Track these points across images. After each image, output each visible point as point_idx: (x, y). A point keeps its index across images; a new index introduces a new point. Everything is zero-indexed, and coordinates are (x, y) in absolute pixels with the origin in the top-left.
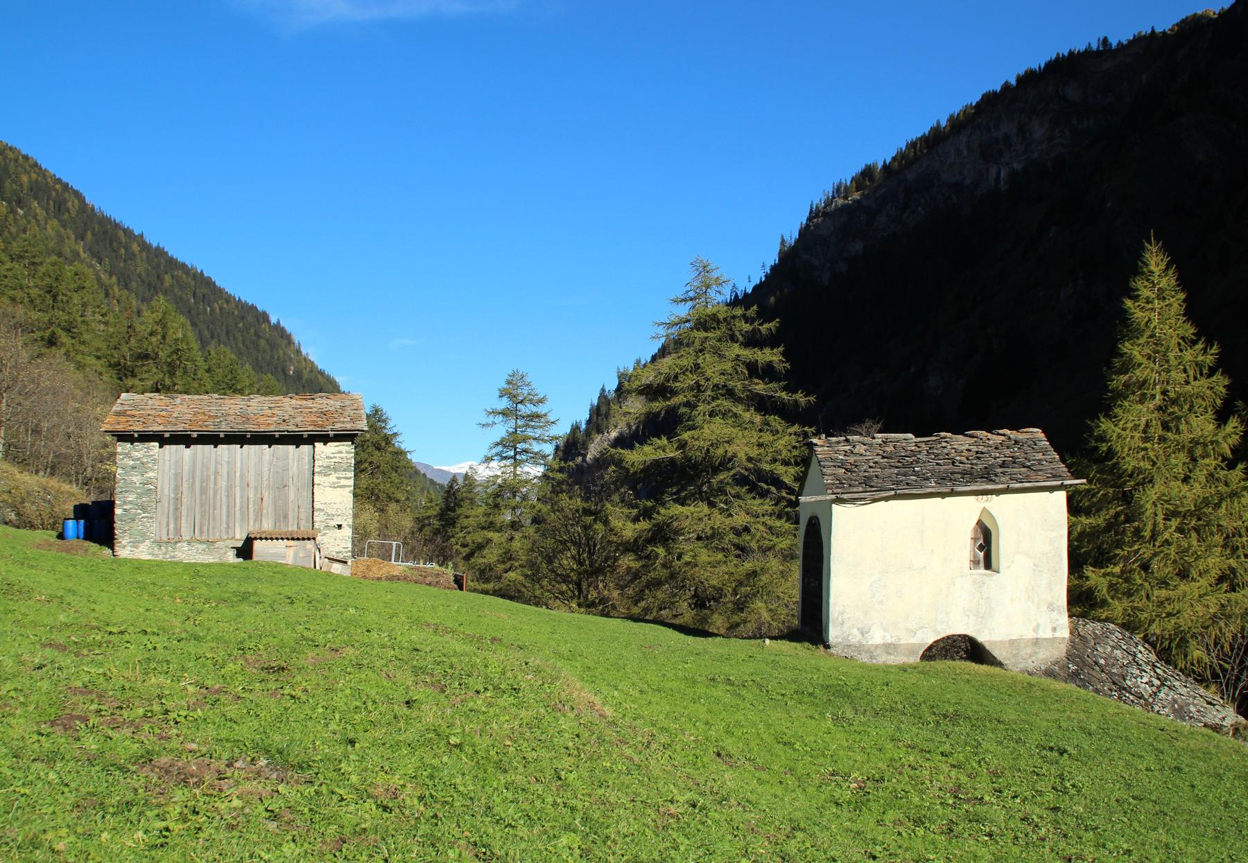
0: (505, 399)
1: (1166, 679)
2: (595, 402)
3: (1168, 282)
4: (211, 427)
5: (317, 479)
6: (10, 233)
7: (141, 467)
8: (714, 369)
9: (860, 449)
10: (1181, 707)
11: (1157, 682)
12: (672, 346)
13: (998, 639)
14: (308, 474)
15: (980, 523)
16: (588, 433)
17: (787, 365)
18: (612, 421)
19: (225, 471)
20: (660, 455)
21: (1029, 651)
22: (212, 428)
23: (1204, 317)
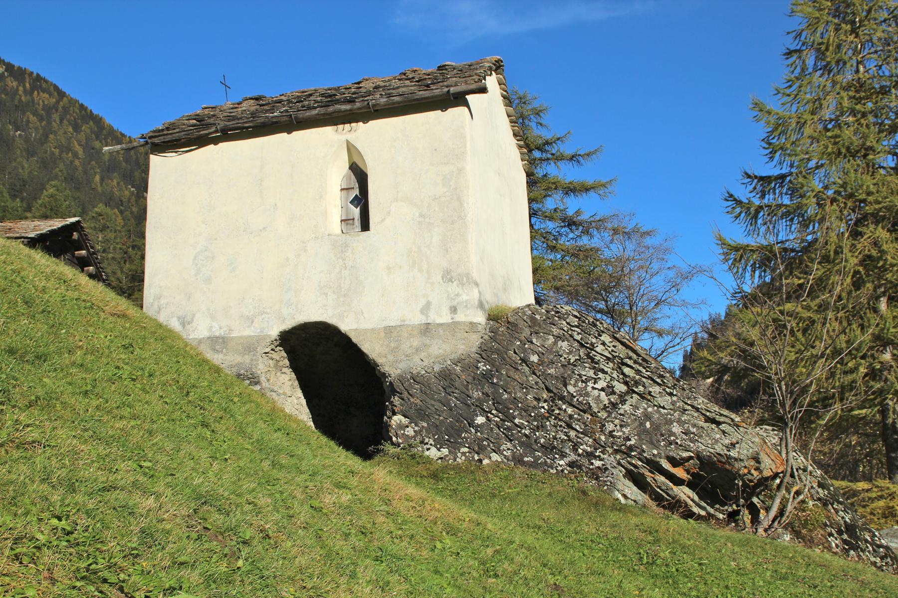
1: (637, 383)
6: (132, 213)
10: (656, 427)
11: (620, 388)
13: (369, 326)
15: (351, 168)
21: (416, 343)
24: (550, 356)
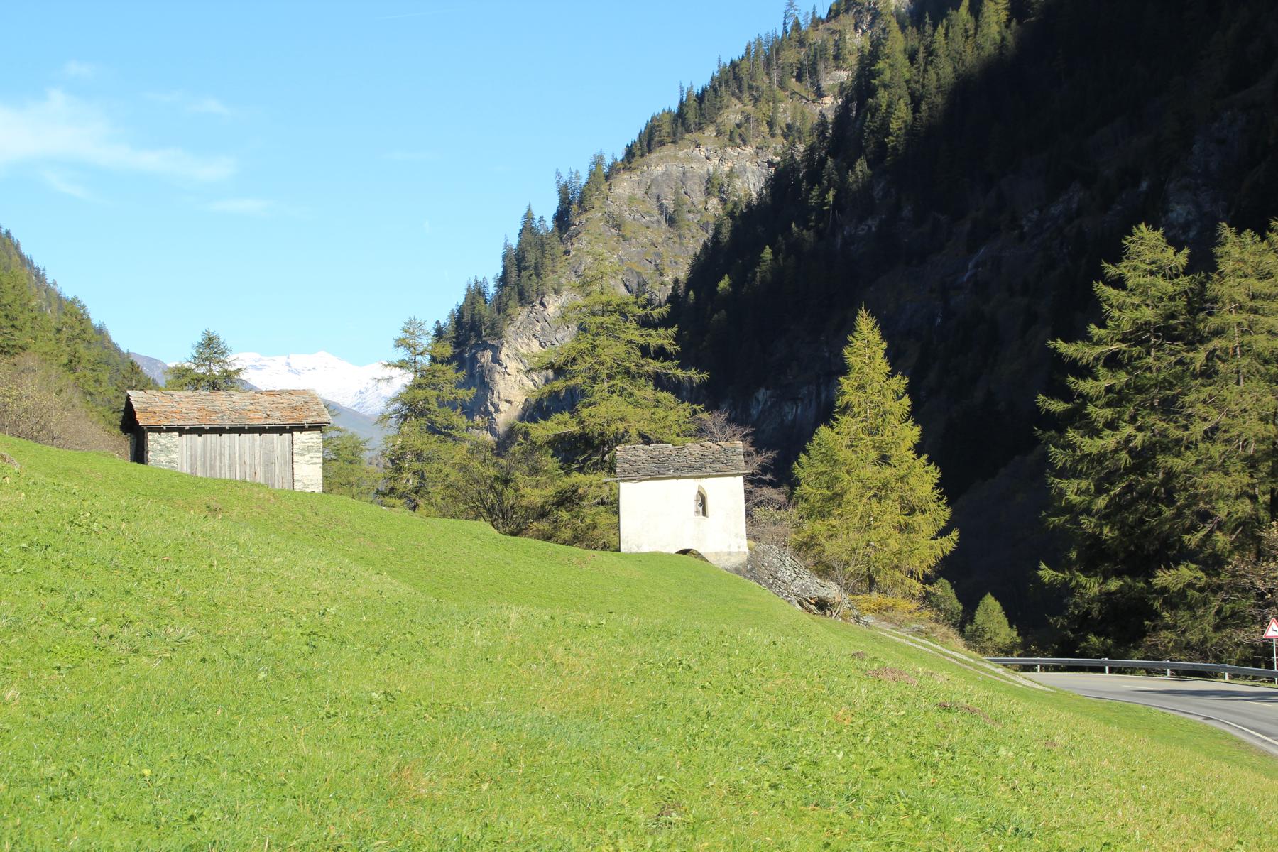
0: (401, 349)
2: (514, 242)
3: (876, 336)
4: (239, 422)
5: (295, 458)
7: (166, 450)
8: (611, 350)
9: (641, 453)
12: (667, 128)
14: (288, 455)
16: (501, 306)
17: (678, 348)
18: (550, 280)
19: (227, 452)
20: (562, 430)
22: (219, 422)
23: (895, 359)
24: (771, 564)
